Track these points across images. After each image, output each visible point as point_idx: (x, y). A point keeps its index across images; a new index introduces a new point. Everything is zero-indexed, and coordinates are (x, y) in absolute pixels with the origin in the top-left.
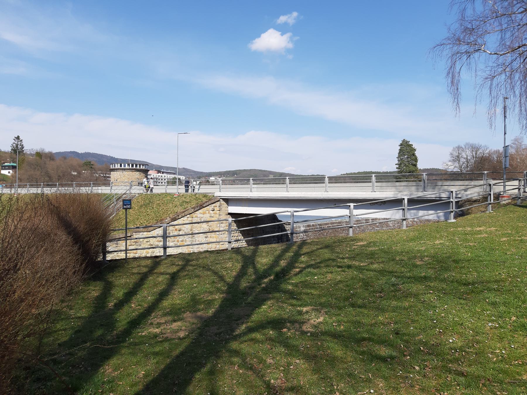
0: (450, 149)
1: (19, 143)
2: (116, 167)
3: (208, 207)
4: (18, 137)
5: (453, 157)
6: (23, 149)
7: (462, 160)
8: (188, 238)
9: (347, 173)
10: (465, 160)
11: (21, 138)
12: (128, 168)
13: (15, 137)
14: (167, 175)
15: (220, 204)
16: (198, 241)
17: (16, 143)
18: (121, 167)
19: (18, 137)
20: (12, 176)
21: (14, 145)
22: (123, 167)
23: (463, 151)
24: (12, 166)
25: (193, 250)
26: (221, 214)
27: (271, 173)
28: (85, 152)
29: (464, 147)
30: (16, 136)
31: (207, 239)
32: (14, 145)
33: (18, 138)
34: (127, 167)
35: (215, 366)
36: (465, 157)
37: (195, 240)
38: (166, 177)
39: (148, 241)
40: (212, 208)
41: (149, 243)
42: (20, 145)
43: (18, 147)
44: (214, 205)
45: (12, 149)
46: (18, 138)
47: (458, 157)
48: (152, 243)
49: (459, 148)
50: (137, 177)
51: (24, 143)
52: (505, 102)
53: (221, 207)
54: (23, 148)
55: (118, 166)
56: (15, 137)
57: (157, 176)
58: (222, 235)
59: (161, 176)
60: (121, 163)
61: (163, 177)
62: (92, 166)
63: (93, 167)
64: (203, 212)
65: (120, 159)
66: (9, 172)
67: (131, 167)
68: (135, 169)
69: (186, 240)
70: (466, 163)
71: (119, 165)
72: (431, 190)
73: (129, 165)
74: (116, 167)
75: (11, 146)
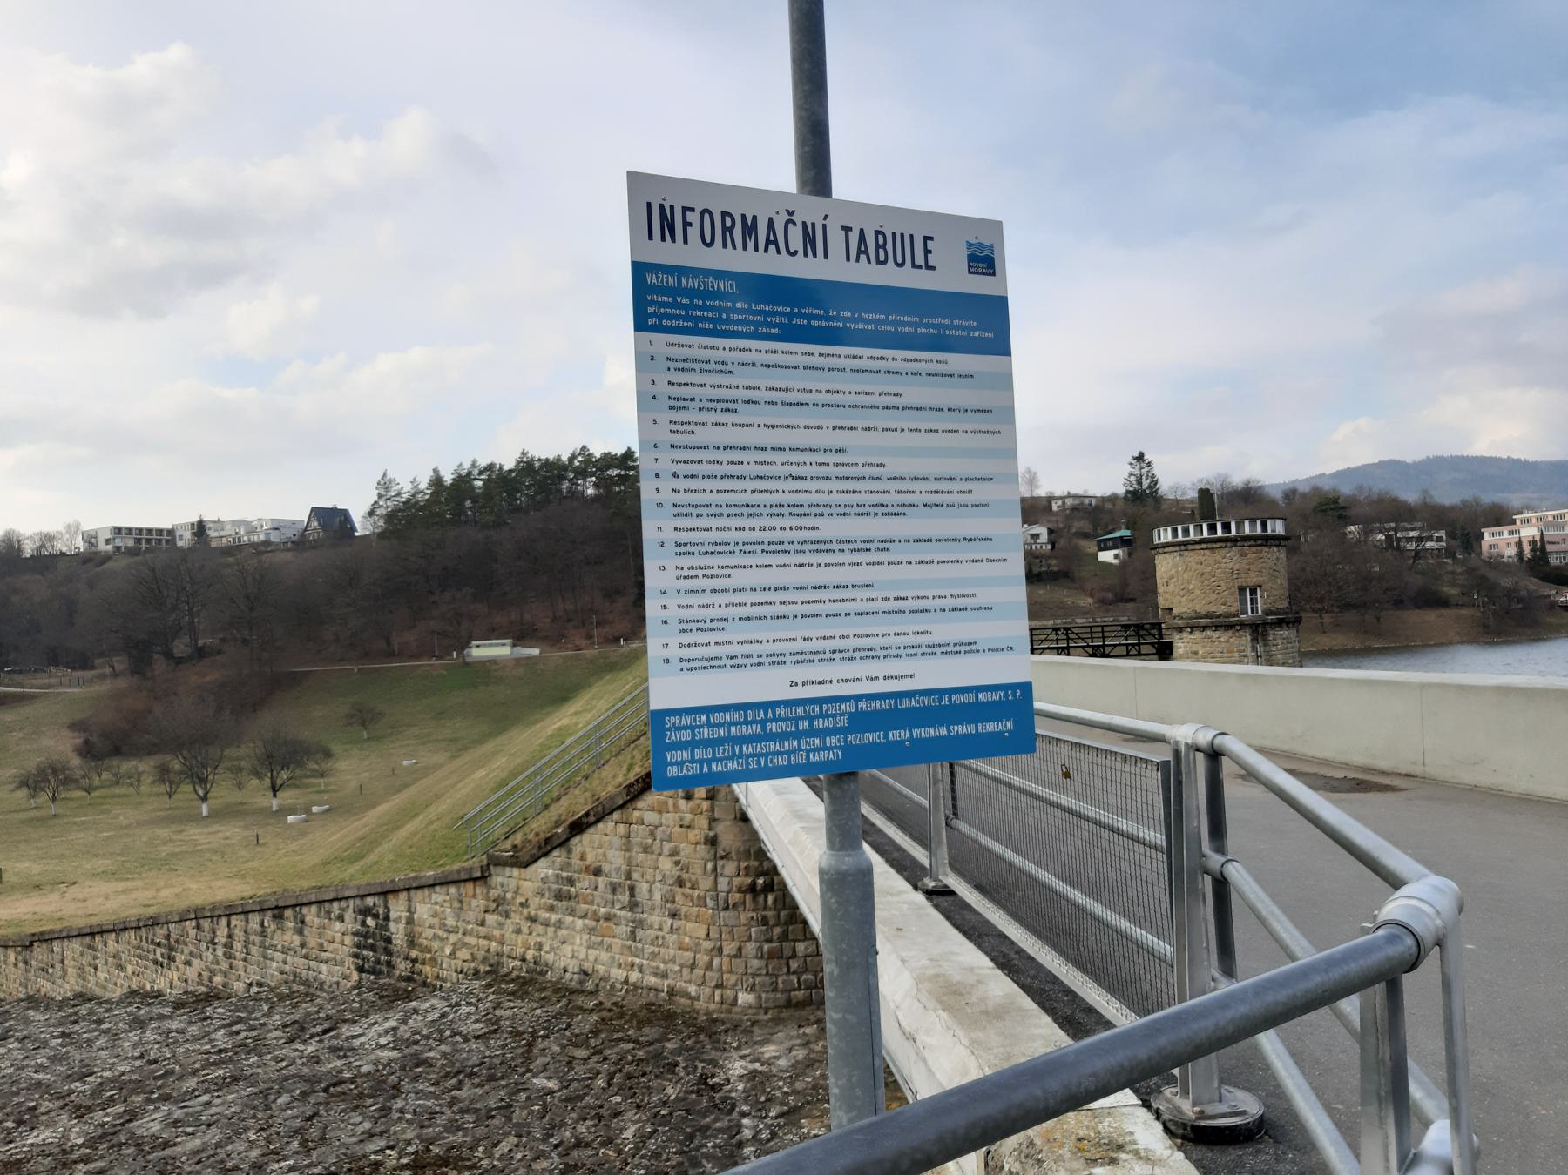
1: (1144, 471)
17: (1137, 472)
18: (1189, 535)
21: (1133, 478)
22: (1180, 537)
24: (1121, 537)
26: (716, 816)
28: (1424, 457)
30: (1136, 455)
33: (1140, 458)
34: (1247, 530)
35: (1197, 1118)
42: (1147, 477)
50: (1231, 565)
51: (1157, 471)
55: (1166, 537)
58: (727, 914)
60: (1226, 519)
62: (1341, 512)
63: (1344, 513)
66: (1116, 556)
67: (1206, 534)
68: (1219, 540)
71: (1169, 529)
72: (1202, 912)
73: (1253, 524)
74: (1163, 540)
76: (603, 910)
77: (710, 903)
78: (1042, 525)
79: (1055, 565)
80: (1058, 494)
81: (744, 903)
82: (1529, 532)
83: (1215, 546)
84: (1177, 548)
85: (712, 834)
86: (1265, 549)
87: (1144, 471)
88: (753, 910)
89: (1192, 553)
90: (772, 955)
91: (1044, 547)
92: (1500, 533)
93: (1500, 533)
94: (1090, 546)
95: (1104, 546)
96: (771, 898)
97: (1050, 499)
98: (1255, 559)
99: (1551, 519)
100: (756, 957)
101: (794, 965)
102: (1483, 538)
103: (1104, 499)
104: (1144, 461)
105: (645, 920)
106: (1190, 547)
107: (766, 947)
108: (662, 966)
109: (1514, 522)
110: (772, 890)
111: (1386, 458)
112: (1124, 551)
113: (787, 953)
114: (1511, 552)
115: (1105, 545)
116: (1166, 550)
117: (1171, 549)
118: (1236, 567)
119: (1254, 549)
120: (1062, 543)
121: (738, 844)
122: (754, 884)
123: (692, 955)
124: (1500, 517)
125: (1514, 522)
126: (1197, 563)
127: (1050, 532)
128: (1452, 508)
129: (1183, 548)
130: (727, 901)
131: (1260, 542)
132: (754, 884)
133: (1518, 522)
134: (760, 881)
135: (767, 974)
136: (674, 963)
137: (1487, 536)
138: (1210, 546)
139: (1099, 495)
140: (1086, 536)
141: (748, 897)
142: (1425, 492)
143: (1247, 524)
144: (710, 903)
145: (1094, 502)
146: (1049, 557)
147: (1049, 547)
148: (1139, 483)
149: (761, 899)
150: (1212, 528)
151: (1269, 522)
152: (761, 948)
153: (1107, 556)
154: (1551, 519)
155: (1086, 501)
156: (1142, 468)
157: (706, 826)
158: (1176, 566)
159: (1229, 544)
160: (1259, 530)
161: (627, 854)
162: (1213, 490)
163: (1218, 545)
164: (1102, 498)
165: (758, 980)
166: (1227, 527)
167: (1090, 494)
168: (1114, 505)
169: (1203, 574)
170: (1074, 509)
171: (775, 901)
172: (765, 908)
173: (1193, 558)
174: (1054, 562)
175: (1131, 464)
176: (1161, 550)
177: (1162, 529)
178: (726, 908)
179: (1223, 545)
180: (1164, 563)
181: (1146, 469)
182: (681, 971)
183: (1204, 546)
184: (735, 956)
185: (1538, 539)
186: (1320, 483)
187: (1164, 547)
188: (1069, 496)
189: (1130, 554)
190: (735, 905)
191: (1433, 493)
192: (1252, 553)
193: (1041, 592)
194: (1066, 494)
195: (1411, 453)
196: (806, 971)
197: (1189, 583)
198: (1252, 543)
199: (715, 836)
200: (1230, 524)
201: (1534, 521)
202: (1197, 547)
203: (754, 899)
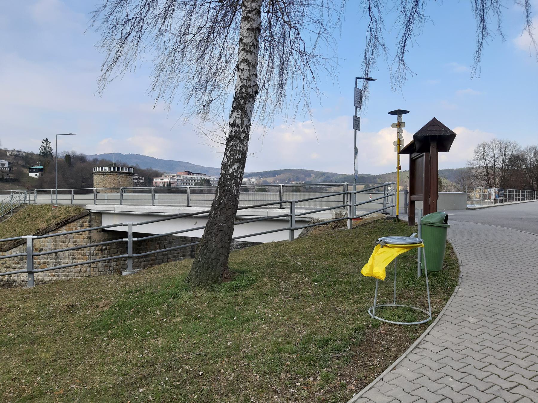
0: (473, 148)
1: (48, 145)
2: (97, 171)
3: (75, 223)
4: (47, 140)
5: (478, 156)
6: (52, 152)
7: (488, 158)
8: (51, 260)
9: (392, 172)
10: (491, 159)
11: (49, 141)
12: (110, 171)
13: (44, 140)
14: (197, 176)
15: (91, 218)
16: (64, 263)
17: (45, 145)
18: (115, 170)
19: (47, 140)
20: (39, 178)
21: (43, 147)
23: (489, 148)
24: (39, 168)
25: (57, 274)
27: (313, 172)
29: (490, 144)
30: (45, 139)
31: (74, 261)
32: (43, 147)
33: (46, 140)
36: (492, 155)
37: (60, 262)
38: (196, 178)
39: (4, 262)
40: (80, 224)
41: (4, 265)
42: (48, 148)
43: (46, 150)
44: (82, 220)
45: (41, 152)
46: (46, 140)
47: (483, 155)
48: (8, 265)
49: (484, 145)
50: (119, 180)
52: (298, 32)
53: (92, 222)
54: (51, 151)
56: (44, 140)
57: (187, 178)
58: (93, 256)
59: (191, 177)
61: (193, 178)
64: (69, 228)
65: (163, 160)
66: (36, 175)
68: (116, 172)
69: (48, 262)
70: (492, 161)
71: (100, 168)
73: (126, 169)
75: (40, 149)
76: (42, 261)
77: (88, 254)
78: (6, 160)
79: (12, 176)
80: (9, 149)
81: (99, 253)
82: (166, 180)
83: (115, 174)
84: (103, 174)
85: (90, 236)
86: (129, 176)
87: (48, 145)
88: (101, 255)
89: (107, 176)
90: (106, 266)
91: (7, 169)
92: (158, 179)
93: (158, 179)
94: (26, 171)
95: (32, 171)
96: (106, 252)
97: (6, 151)
98: (126, 179)
99: (172, 176)
100: (102, 267)
101: (111, 268)
102: (153, 180)
103: (28, 154)
104: (48, 142)
105: (61, 261)
106: (107, 174)
107: (104, 264)
108: (67, 274)
109: (161, 177)
110: (107, 250)
111: (116, 152)
112: (39, 173)
113: (109, 265)
114: (161, 185)
115: (32, 171)
116: (99, 174)
117: (100, 174)
118: (121, 181)
119: (126, 176)
120: (14, 168)
121: (98, 238)
122: (102, 248)
123: (80, 269)
124: (158, 175)
125: (161, 177)
126: (109, 179)
127: (10, 163)
128: (145, 170)
129: (105, 174)
130: (93, 253)
131: (127, 174)
132: (102, 248)
133: (163, 177)
134: (104, 247)
135: (104, 271)
136: (73, 272)
137: (154, 180)
138: (113, 174)
139: (26, 151)
140: (23, 166)
141: (100, 252)
142: (137, 165)
143: (124, 168)
144: (88, 254)
145: (24, 154)
146: (9, 173)
147: (9, 169)
148: (45, 149)
149: (104, 252)
150: (114, 169)
151: (130, 169)
152: (103, 264)
153: (33, 175)
154: (172, 176)
155: (21, 153)
156: (46, 144)
157: (88, 234)
158: (101, 179)
159: (119, 174)
160: (127, 171)
161: (55, 244)
162: (70, 155)
163: (116, 174)
164: (27, 153)
165: (101, 273)
166: (118, 169)
167: (22, 151)
168: (32, 156)
169: (110, 182)
170: (17, 156)
171: (107, 253)
172: (105, 254)
173: (107, 177)
174: (11, 175)
175: (43, 142)
176: (97, 174)
177: (97, 168)
178: (93, 255)
179: (117, 174)
180: (98, 178)
181: (48, 145)
182: (75, 274)
183: (111, 174)
184: (95, 267)
185: (169, 182)
186: (105, 158)
187: (98, 173)
188: (14, 150)
189: (42, 175)
190: (96, 254)
191: (140, 165)
192: (125, 177)
193: (7, 186)
194: (13, 150)
195: (125, 152)
196: (114, 270)
197: (106, 185)
198: (125, 174)
199: (91, 236)
200: (119, 168)
201: (167, 177)
202: (109, 174)
203: (102, 252)
